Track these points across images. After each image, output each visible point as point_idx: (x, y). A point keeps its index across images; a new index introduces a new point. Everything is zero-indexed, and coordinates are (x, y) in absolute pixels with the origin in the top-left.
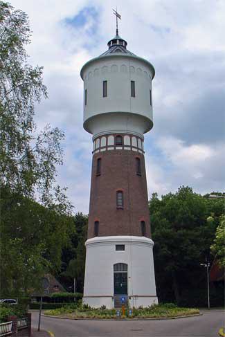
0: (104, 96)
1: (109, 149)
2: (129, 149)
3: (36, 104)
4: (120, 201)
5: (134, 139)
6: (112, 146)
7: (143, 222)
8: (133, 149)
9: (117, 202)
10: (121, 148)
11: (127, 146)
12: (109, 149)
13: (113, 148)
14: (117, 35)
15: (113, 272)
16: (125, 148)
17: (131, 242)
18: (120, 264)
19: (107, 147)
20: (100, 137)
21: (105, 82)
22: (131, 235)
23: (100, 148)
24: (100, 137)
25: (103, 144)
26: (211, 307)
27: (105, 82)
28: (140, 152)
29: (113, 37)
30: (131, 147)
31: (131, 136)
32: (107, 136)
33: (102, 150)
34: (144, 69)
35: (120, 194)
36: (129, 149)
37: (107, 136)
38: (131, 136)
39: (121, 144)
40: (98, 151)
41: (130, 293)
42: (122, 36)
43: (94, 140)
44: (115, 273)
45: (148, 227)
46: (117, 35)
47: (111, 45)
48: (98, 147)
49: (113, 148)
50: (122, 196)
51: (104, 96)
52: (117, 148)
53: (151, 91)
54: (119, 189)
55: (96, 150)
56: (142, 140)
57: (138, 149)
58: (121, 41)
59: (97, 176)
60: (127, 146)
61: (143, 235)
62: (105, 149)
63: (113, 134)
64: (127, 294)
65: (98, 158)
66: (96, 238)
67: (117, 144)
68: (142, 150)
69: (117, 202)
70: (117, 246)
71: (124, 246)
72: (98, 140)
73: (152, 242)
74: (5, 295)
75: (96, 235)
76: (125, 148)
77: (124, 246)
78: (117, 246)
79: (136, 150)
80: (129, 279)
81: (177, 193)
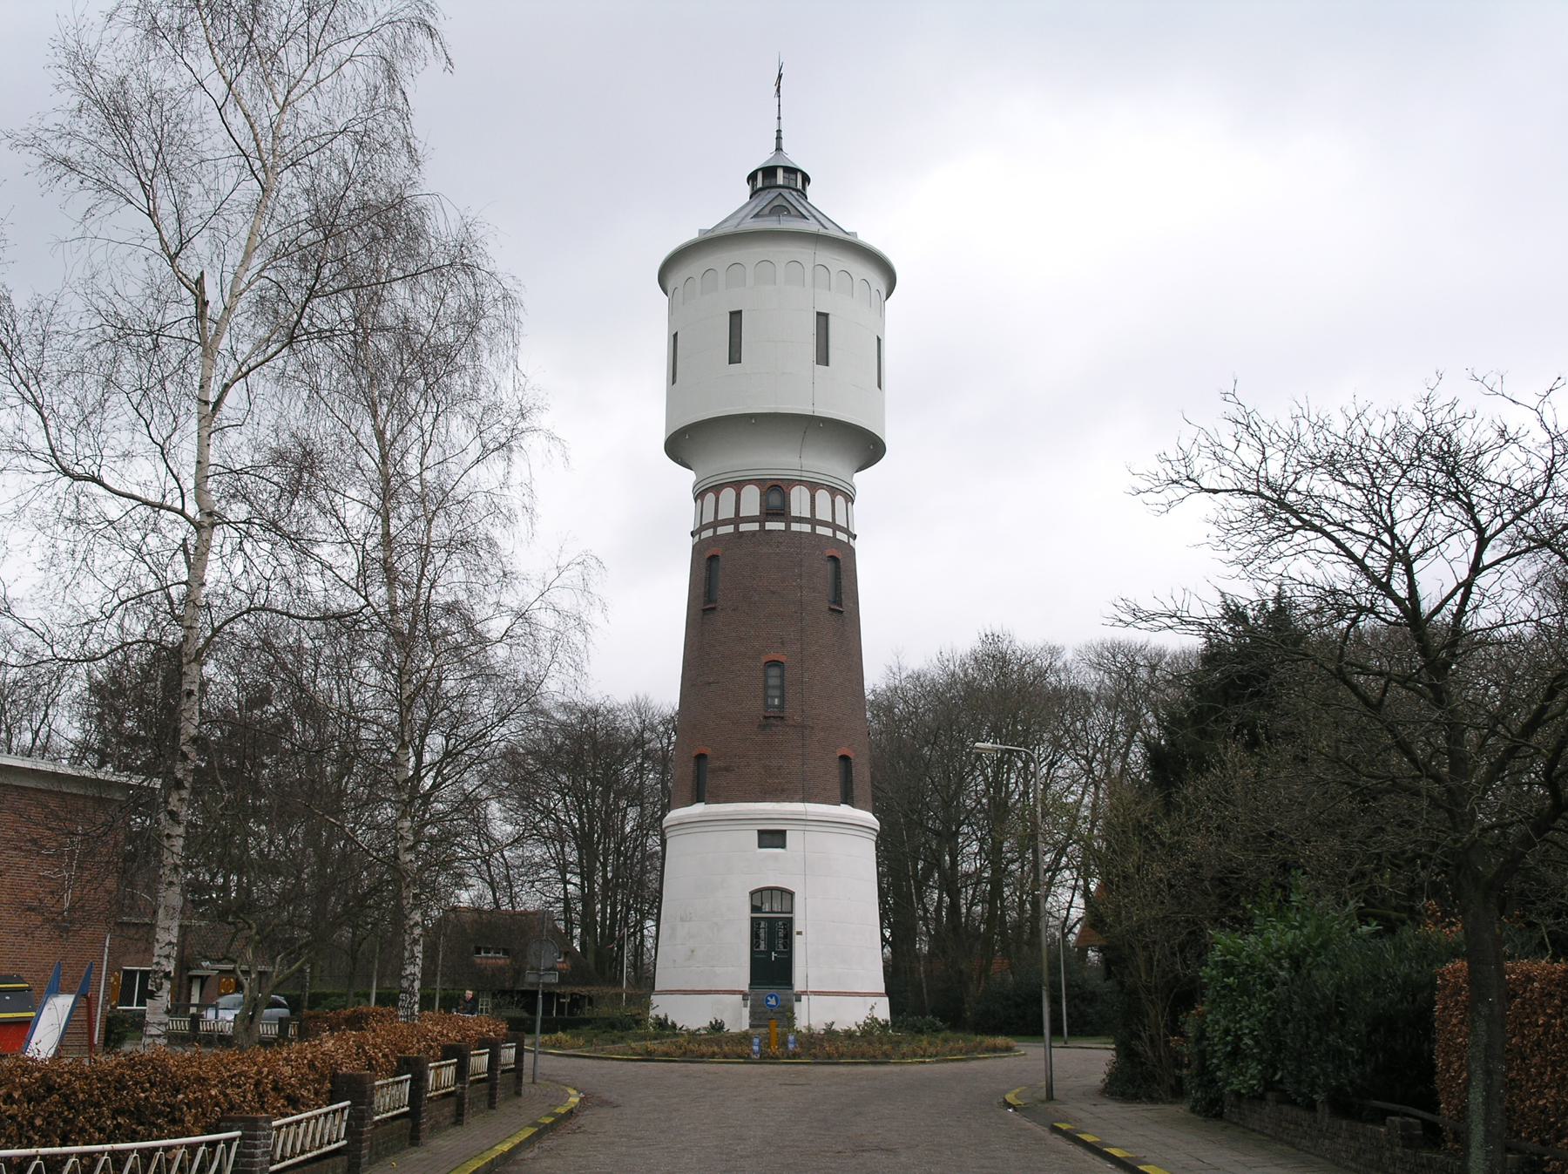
2: (807, 528)
5: (823, 497)
6: (726, 522)
8: (820, 530)
10: (781, 526)
11: (800, 520)
12: (743, 527)
13: (755, 527)
16: (795, 527)
18: (771, 889)
19: (737, 520)
25: (727, 512)
26: (1069, 1034)
28: (841, 536)
30: (813, 521)
31: (813, 487)
32: (738, 485)
33: (722, 530)
35: (774, 672)
36: (807, 528)
37: (738, 485)
38: (813, 487)
49: (755, 527)
50: (782, 677)
52: (770, 526)
58: (791, 171)
60: (800, 520)
61: (847, 798)
62: (730, 529)
66: (699, 809)
71: (783, 833)
72: (710, 497)
73: (876, 824)
76: (795, 527)
77: (783, 833)
79: (828, 532)
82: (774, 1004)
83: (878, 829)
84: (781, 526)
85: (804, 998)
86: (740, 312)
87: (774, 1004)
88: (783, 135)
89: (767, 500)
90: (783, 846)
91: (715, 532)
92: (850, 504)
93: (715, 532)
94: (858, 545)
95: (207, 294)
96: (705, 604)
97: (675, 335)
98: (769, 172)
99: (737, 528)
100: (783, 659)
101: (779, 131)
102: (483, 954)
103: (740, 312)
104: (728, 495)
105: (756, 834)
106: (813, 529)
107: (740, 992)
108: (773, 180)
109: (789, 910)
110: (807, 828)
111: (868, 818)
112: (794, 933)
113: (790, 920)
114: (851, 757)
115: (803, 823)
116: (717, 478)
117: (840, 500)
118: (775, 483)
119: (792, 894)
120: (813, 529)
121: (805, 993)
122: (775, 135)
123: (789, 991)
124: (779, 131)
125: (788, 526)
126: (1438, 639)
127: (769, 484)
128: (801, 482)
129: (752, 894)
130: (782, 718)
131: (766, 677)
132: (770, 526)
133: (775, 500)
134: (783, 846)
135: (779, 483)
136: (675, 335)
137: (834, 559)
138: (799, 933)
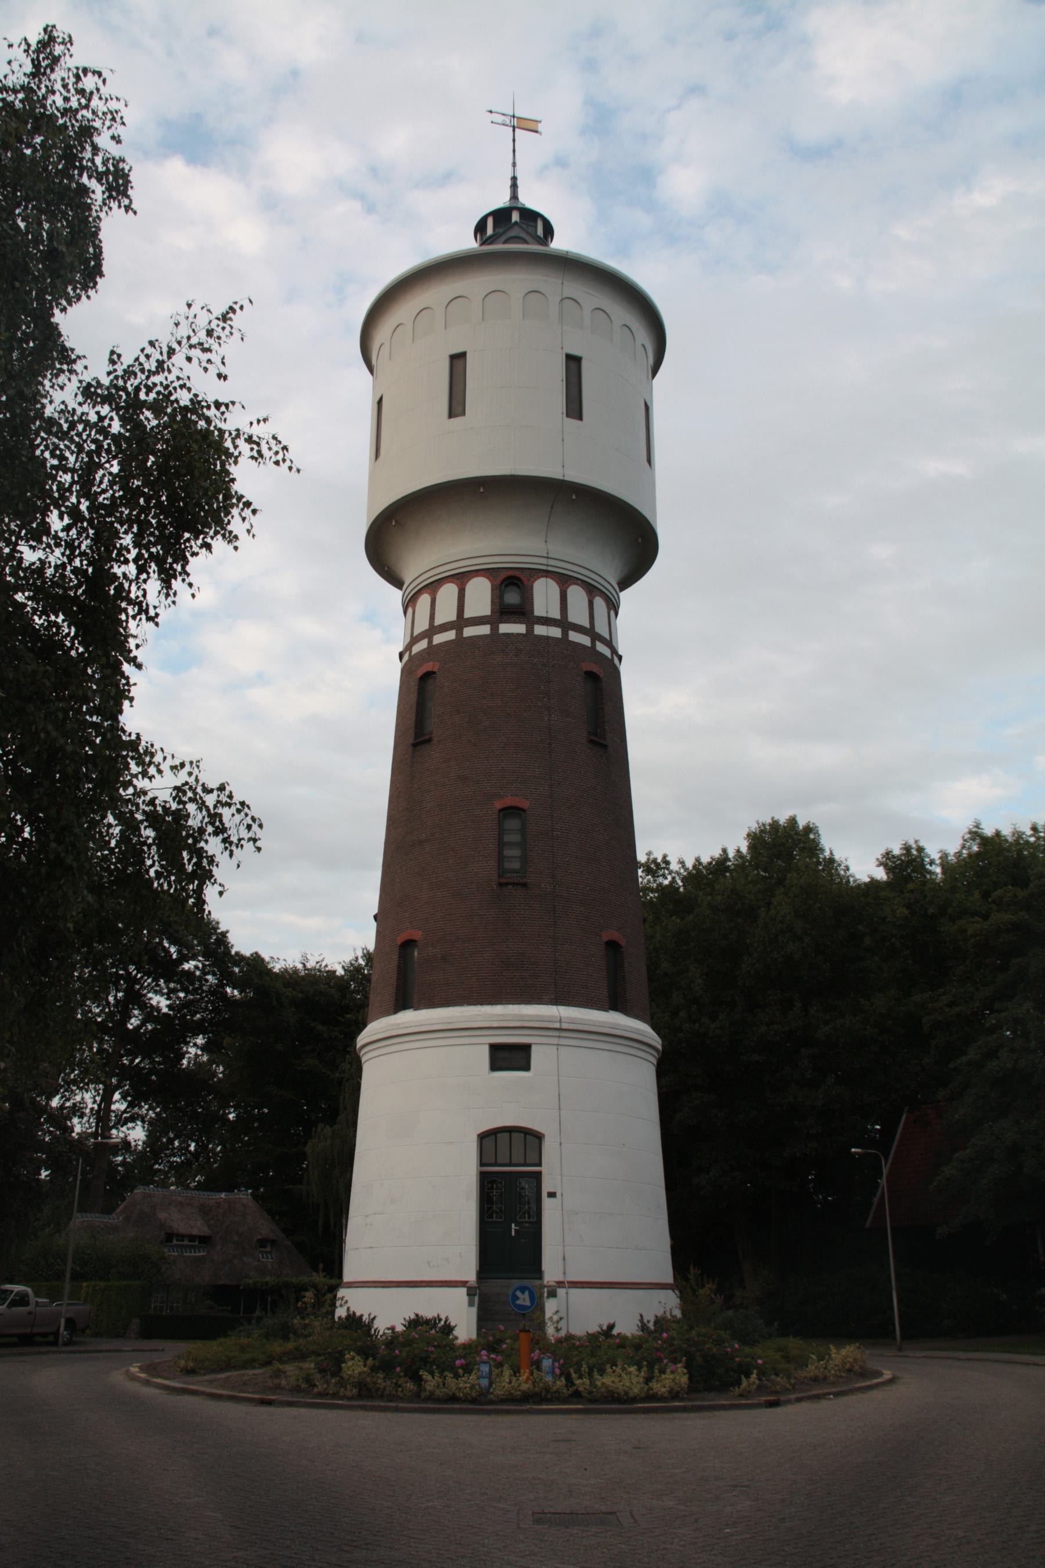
2: (555, 632)
4: (515, 852)
5: (577, 595)
6: (444, 628)
7: (612, 946)
8: (574, 637)
9: (501, 858)
10: (520, 629)
11: (546, 621)
12: (469, 632)
13: (485, 630)
15: (545, 1169)
16: (540, 630)
17: (561, 1030)
18: (510, 1130)
19: (461, 622)
20: (432, 587)
21: (458, 359)
22: (556, 1001)
23: (433, 630)
24: (432, 587)
25: (446, 613)
26: (903, 1338)
27: (458, 359)
28: (601, 648)
29: (502, 200)
30: (564, 624)
31: (564, 581)
32: (461, 579)
33: (439, 639)
34: (621, 314)
35: (513, 824)
36: (555, 632)
37: (461, 579)
38: (564, 581)
39: (522, 612)
40: (423, 645)
41: (551, 1271)
42: (528, 200)
43: (409, 604)
44: (540, 1164)
45: (636, 971)
47: (490, 231)
48: (422, 625)
49: (485, 630)
50: (523, 831)
52: (505, 628)
53: (647, 408)
54: (509, 801)
55: (414, 640)
56: (613, 606)
57: (595, 637)
58: (530, 216)
59: (415, 745)
60: (546, 621)
61: (616, 1003)
62: (450, 635)
63: (487, 573)
64: (538, 1273)
65: (420, 673)
66: (408, 1018)
67: (503, 612)
68: (609, 644)
69: (501, 858)
70: (494, 1048)
71: (526, 1048)
72: (425, 600)
73: (656, 1041)
74: (4, 187)
75: (402, 1002)
76: (540, 630)
77: (526, 1048)
78: (494, 1048)
79: (585, 640)
80: (549, 1206)
81: (655, 868)
82: (528, 1303)
83: (660, 1047)
84: (520, 629)
85: (561, 1292)
86: (463, 355)
87: (528, 1303)
88: (519, 183)
89: (501, 597)
90: (526, 1067)
91: (430, 642)
92: (612, 613)
93: (430, 642)
94: (626, 671)
95: (232, 938)
96: (416, 738)
97: (380, 402)
98: (501, 216)
99: (495, 629)
100: (525, 804)
101: (514, 179)
102: (175, 1242)
103: (463, 355)
104: (448, 593)
105: (485, 1052)
106: (565, 634)
107: (463, 1284)
109: (537, 1161)
111: (640, 1028)
112: (544, 1195)
113: (538, 1176)
114: (623, 944)
117: (599, 603)
118: (511, 573)
119: (539, 1137)
120: (565, 634)
121: (560, 1284)
122: (509, 183)
123: (537, 1282)
124: (514, 179)
125: (530, 630)
127: (504, 575)
128: (547, 574)
129: (483, 1137)
130: (524, 885)
131: (501, 831)
132: (505, 628)
133: (512, 598)
134: (526, 1067)
135: (518, 574)
136: (380, 402)
137: (591, 676)
138: (552, 1195)
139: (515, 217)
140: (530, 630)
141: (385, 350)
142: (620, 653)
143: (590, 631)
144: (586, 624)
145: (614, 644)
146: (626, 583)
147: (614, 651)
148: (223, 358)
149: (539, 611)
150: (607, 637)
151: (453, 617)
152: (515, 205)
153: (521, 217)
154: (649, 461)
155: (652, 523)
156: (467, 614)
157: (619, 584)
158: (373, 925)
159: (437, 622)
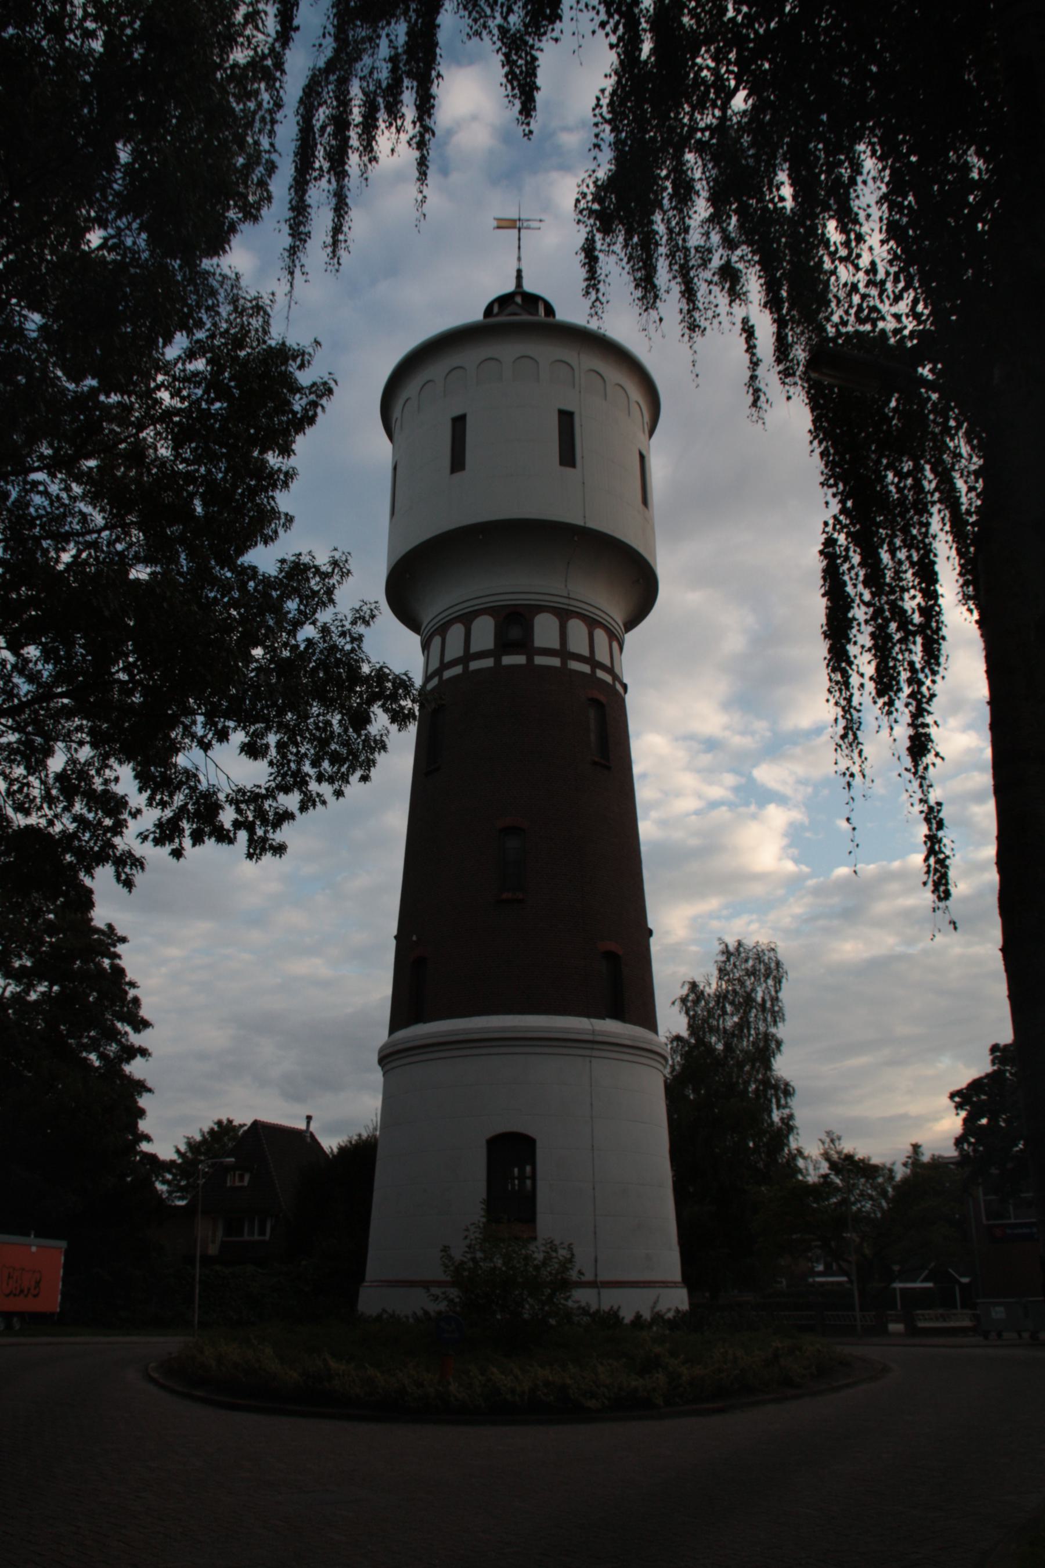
0: (453, 470)
1: (474, 665)
2: (555, 662)
3: (281, 531)
5: (577, 630)
6: (481, 655)
8: (575, 665)
10: (520, 660)
12: (474, 665)
13: (489, 663)
14: (596, 1275)
16: (539, 660)
19: (468, 657)
21: (459, 423)
22: (588, 1015)
24: (442, 630)
25: (455, 649)
27: (459, 423)
28: (601, 674)
31: (564, 615)
32: (467, 619)
33: (448, 674)
36: (555, 662)
37: (467, 619)
39: (525, 645)
42: (528, 287)
46: (599, 1294)
48: (435, 664)
49: (489, 663)
51: (453, 470)
52: (507, 660)
53: (642, 458)
57: (596, 664)
62: (458, 670)
67: (504, 645)
68: (610, 670)
72: (437, 641)
76: (539, 660)
84: (520, 660)
92: (615, 645)
98: (504, 301)
99: (498, 661)
101: (519, 272)
104: (457, 631)
106: (564, 663)
108: (824, 334)
110: (595, 1053)
115: (589, 1045)
116: (446, 613)
120: (564, 663)
122: (515, 274)
124: (519, 272)
125: (530, 660)
126: (699, 117)
132: (507, 660)
133: (515, 633)
139: (519, 299)
140: (530, 660)
141: (398, 423)
142: (625, 680)
143: (591, 660)
144: (586, 653)
145: (617, 670)
146: (632, 623)
147: (616, 678)
148: (955, 928)
149: (540, 641)
150: (608, 664)
151: (460, 653)
152: (519, 290)
153: (523, 300)
154: (645, 501)
155: (641, 550)
156: (474, 648)
157: (625, 625)
158: (394, 942)
159: (447, 659)
